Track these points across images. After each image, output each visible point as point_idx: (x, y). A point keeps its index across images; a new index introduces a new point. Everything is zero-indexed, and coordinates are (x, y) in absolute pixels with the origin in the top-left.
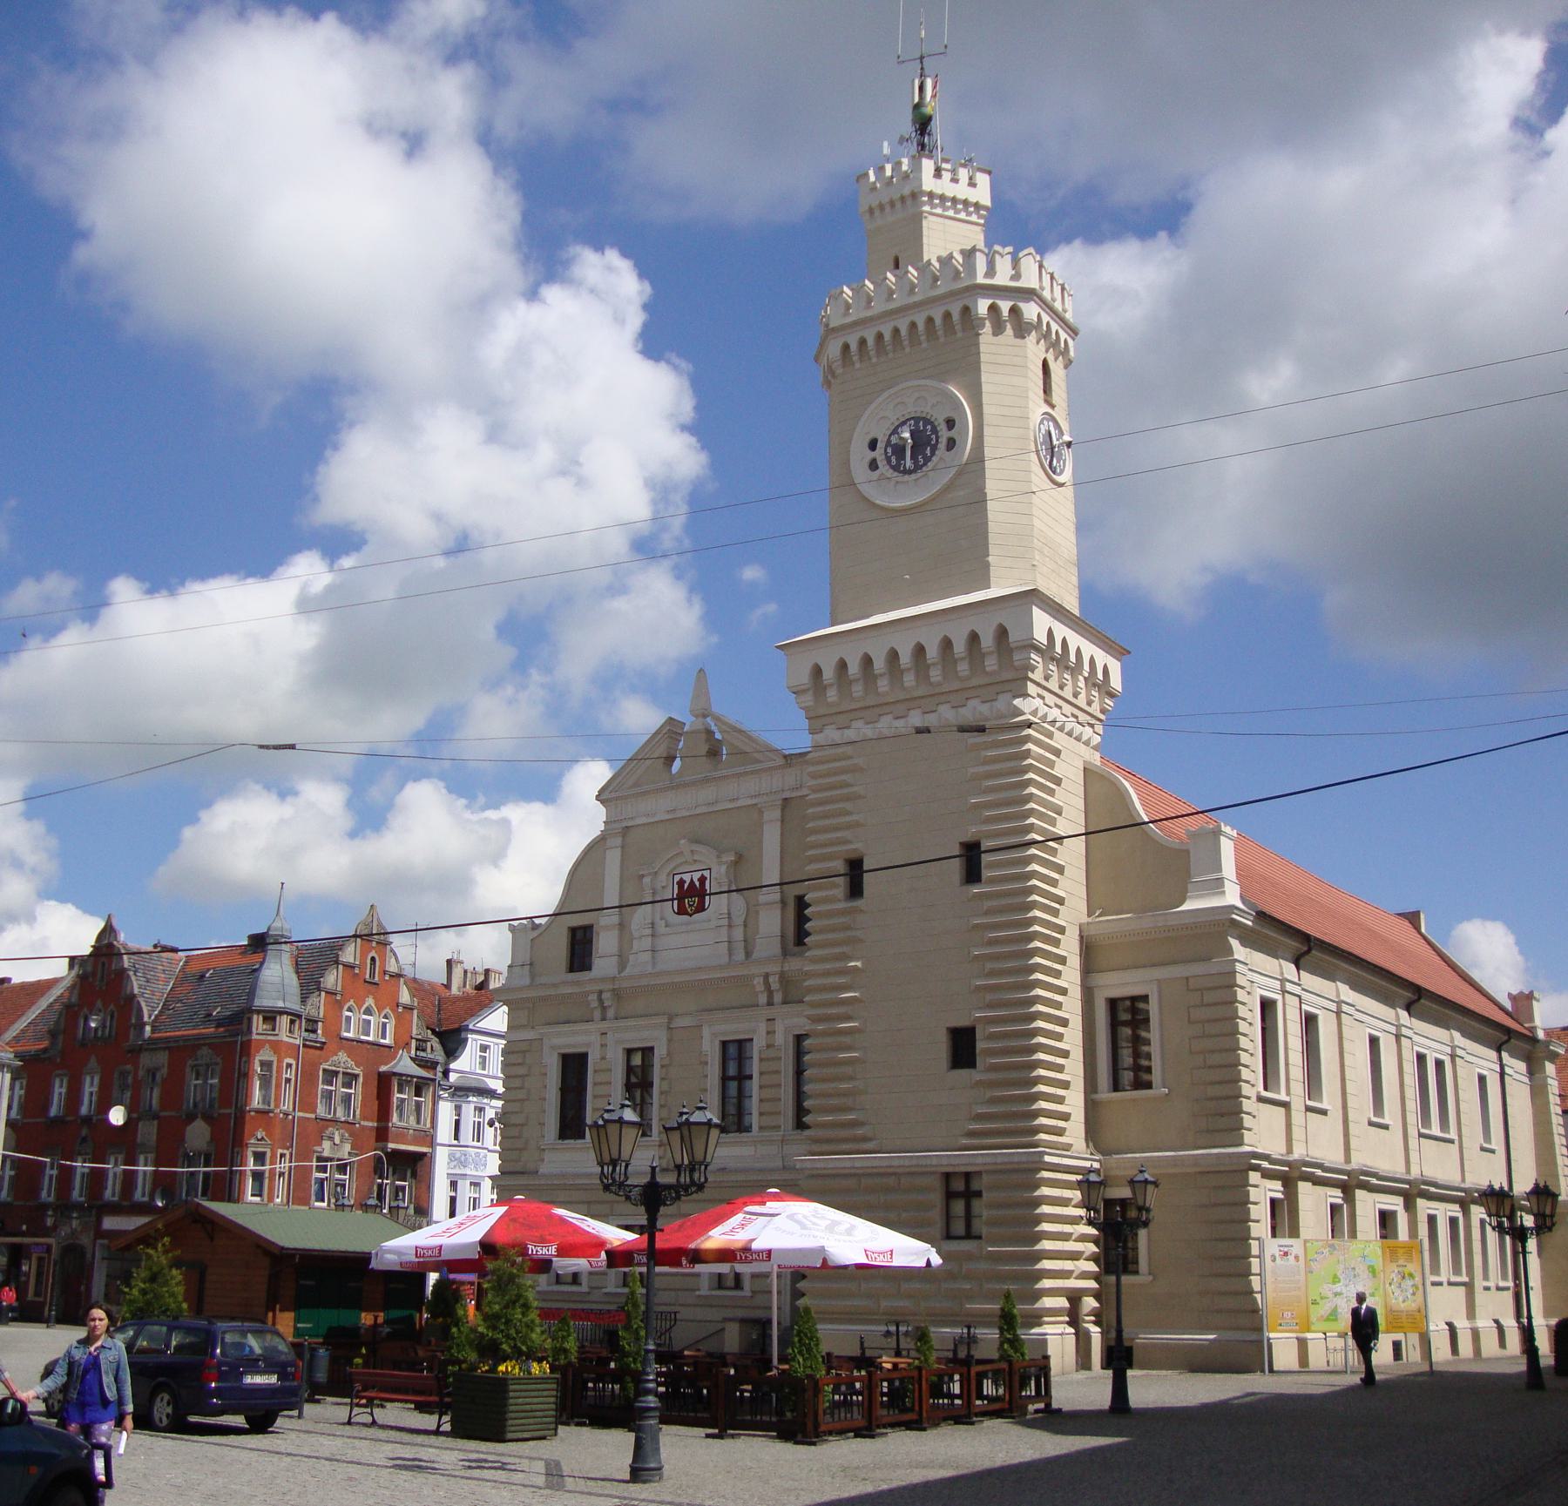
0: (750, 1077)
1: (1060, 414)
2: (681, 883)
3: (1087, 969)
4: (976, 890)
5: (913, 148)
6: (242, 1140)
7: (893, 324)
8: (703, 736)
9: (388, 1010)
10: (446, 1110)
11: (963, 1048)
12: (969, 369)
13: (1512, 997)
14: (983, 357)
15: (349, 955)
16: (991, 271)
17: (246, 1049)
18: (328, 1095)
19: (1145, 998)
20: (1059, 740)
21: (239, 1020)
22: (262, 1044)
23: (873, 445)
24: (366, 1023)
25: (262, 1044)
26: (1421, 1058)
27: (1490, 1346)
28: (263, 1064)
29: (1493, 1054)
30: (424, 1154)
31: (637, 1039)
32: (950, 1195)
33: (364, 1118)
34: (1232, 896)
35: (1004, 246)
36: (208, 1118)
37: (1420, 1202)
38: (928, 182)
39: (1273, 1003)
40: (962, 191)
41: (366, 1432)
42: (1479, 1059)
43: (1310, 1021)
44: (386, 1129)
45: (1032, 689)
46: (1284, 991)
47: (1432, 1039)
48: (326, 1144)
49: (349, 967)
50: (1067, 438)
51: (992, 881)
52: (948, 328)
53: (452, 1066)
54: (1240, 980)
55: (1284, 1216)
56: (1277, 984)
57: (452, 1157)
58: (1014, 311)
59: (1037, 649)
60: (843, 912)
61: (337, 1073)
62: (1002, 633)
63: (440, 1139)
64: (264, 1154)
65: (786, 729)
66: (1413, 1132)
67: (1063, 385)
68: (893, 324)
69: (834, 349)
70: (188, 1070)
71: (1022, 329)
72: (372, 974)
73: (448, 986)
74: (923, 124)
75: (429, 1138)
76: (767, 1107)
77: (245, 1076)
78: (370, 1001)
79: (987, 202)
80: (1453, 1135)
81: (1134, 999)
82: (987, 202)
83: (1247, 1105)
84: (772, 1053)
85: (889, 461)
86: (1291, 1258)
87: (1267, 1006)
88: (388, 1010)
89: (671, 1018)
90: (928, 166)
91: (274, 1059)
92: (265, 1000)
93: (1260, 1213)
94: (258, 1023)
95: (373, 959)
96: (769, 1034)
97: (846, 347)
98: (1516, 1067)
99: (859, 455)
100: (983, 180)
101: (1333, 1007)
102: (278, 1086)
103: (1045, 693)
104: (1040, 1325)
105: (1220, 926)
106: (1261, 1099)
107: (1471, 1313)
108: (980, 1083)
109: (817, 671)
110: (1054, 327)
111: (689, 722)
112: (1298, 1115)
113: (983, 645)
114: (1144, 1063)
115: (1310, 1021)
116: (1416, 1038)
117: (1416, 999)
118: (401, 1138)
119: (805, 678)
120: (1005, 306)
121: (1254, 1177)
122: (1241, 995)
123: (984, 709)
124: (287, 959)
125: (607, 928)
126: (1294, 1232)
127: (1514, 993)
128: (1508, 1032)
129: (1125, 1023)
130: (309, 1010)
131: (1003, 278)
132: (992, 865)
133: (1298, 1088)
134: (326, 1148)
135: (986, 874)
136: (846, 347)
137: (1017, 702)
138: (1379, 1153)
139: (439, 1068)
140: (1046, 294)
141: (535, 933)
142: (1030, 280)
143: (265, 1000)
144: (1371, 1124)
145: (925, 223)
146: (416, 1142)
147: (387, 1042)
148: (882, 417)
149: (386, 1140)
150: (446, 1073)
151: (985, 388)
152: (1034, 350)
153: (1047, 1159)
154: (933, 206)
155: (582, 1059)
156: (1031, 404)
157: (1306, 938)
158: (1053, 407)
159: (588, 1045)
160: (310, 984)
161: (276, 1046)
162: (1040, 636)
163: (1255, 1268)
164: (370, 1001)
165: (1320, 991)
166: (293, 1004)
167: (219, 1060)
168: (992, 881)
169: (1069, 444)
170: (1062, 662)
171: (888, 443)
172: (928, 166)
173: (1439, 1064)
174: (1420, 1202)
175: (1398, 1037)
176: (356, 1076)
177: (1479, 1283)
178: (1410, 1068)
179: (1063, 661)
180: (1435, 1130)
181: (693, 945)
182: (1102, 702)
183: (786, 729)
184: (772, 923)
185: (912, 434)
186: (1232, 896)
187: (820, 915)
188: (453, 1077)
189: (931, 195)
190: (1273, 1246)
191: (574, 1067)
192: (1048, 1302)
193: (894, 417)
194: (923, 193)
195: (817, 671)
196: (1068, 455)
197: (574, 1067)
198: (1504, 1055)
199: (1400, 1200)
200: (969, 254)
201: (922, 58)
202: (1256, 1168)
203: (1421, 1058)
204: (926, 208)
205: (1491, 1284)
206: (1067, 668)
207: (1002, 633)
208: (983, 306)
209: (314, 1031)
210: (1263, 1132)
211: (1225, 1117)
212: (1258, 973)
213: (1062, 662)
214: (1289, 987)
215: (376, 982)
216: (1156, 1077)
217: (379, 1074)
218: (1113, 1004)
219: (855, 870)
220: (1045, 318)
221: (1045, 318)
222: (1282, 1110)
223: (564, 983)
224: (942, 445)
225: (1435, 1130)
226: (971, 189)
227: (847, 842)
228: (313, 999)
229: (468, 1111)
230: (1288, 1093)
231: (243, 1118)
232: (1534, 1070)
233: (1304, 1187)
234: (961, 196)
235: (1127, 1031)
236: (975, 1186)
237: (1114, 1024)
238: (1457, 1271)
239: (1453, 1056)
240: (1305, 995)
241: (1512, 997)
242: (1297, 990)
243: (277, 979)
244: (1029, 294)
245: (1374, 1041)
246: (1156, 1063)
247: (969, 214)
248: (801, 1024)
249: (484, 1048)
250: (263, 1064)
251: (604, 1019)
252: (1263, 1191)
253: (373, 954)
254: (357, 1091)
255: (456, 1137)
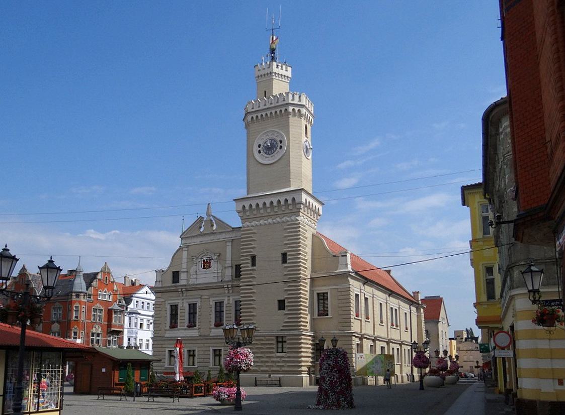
0: (223, 311)
1: (309, 140)
2: (204, 260)
3: (312, 285)
4: (286, 265)
5: (269, 58)
6: (70, 328)
7: (265, 112)
8: (210, 222)
9: (111, 292)
10: (127, 319)
11: (281, 305)
12: (286, 127)
13: (414, 293)
14: (290, 124)
15: (99, 277)
16: (293, 100)
17: (71, 303)
18: (94, 315)
19: (327, 293)
20: (307, 228)
21: (69, 294)
22: (75, 302)
23: (259, 146)
24: (105, 296)
25: (75, 302)
26: (392, 308)
27: (405, 379)
28: (76, 307)
29: (408, 306)
30: (121, 331)
31: (192, 301)
32: (278, 342)
33: (104, 321)
34: (350, 269)
35: (297, 92)
36: (59, 322)
37: (391, 344)
38: (275, 70)
39: (358, 295)
40: (283, 72)
41: (152, 403)
42: (405, 307)
43: (366, 299)
44: (111, 324)
45: (301, 214)
46: (361, 292)
47: (394, 302)
48: (94, 329)
49: (100, 280)
50: (311, 147)
51: (289, 263)
52: (281, 112)
53: (128, 307)
54: (351, 290)
55: (360, 347)
56: (359, 290)
57: (128, 332)
58: (299, 110)
59: (303, 204)
60: (251, 270)
61: (97, 309)
62: (294, 199)
63: (125, 327)
64: (77, 332)
65: (235, 221)
66: (389, 327)
67: (310, 131)
68: (265, 112)
69: (249, 118)
70: (52, 309)
71: (300, 115)
72: (106, 282)
73: (124, 284)
74: (273, 51)
75: (122, 326)
76: (228, 319)
77: (71, 310)
78: (106, 289)
79: (290, 76)
80: (398, 328)
81: (324, 293)
82: (290, 76)
83: (352, 320)
84: (229, 305)
85: (264, 151)
86: (362, 358)
87: (357, 295)
88: (111, 292)
89: (201, 296)
90: (275, 64)
91: (79, 306)
92: (76, 289)
93: (355, 347)
94: (74, 297)
95: (106, 278)
96: (229, 302)
97: (252, 118)
98: (414, 309)
99: (256, 149)
100: (289, 69)
101: (372, 296)
102: (80, 313)
103: (304, 216)
104: (301, 374)
105: (346, 275)
106: (355, 319)
107: (401, 372)
108: (286, 314)
109: (244, 207)
110: (309, 115)
111: (205, 217)
112: (363, 323)
113: (289, 202)
114: (326, 309)
115: (366, 299)
116: (391, 304)
117: (391, 293)
118: (115, 327)
119: (240, 208)
120: (297, 109)
121: (354, 338)
122: (351, 293)
123: (288, 219)
124: (82, 278)
125: (183, 272)
126: (362, 352)
127: (414, 291)
128: (412, 301)
129: (321, 299)
130: (89, 292)
131: (296, 102)
132: (289, 259)
133: (364, 316)
134: (94, 330)
135: (288, 261)
136: (252, 118)
137: (297, 218)
138: (381, 332)
139: (125, 307)
140: (307, 106)
141: (162, 273)
142: (304, 102)
143: (76, 289)
144: (379, 325)
145: (273, 82)
146: (118, 328)
147: (110, 300)
148: (262, 139)
149: (111, 328)
150: (127, 309)
151: (291, 132)
152: (304, 122)
153: (303, 333)
154: (276, 76)
155: (176, 306)
156: (302, 138)
157: (366, 279)
158: (307, 138)
159: (179, 303)
160: (89, 285)
161: (80, 302)
162: (304, 201)
163: (354, 361)
164: (106, 289)
165: (369, 290)
166: (84, 290)
167: (61, 306)
168: (289, 263)
169: (312, 149)
170: (308, 208)
171: (264, 146)
172: (275, 64)
173: (396, 310)
174: (391, 344)
175: (386, 303)
176: (102, 310)
177: (403, 365)
178: (389, 311)
179: (308, 206)
180: (394, 327)
181: (207, 277)
182: (317, 217)
183: (235, 221)
184: (229, 273)
185: (270, 143)
186: (350, 269)
187: (244, 271)
188: (129, 310)
189: (275, 73)
190: (358, 355)
191: (174, 309)
192: (303, 368)
193: (265, 138)
194: (273, 73)
195: (244, 207)
196: (310, 151)
197: (174, 309)
198: (411, 306)
199: (386, 343)
200: (287, 94)
201: (273, 29)
202: (354, 336)
203: (392, 308)
204: (274, 77)
205: (406, 365)
206: (309, 209)
207: (294, 199)
208: (291, 109)
209: (90, 298)
210: (355, 327)
211: (347, 323)
212: (355, 286)
213: (308, 208)
214: (362, 291)
215: (107, 283)
216: (329, 313)
217: (109, 309)
218: (318, 294)
219: (253, 258)
220: (307, 113)
221: (307, 113)
222: (359, 321)
223: (172, 286)
224: (279, 148)
225: (394, 327)
226: (286, 72)
227: (252, 252)
228: (90, 289)
229: (134, 320)
230: (361, 318)
231: (70, 322)
232: (418, 310)
233: (364, 340)
234: (284, 74)
235: (322, 301)
236: (284, 340)
237: (319, 300)
238: (398, 362)
239: (399, 308)
240: (365, 293)
241: (414, 293)
242: (364, 292)
243: (80, 284)
244: (303, 106)
245: (381, 304)
246: (329, 309)
247: (285, 79)
248: (237, 298)
249: (137, 302)
250: (76, 307)
251: (183, 296)
252: (356, 341)
253: (106, 276)
254: (103, 315)
255: (130, 326)
